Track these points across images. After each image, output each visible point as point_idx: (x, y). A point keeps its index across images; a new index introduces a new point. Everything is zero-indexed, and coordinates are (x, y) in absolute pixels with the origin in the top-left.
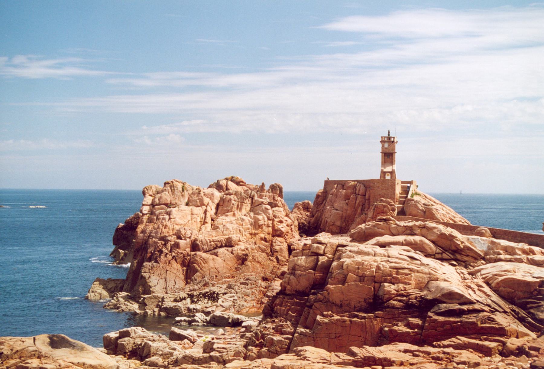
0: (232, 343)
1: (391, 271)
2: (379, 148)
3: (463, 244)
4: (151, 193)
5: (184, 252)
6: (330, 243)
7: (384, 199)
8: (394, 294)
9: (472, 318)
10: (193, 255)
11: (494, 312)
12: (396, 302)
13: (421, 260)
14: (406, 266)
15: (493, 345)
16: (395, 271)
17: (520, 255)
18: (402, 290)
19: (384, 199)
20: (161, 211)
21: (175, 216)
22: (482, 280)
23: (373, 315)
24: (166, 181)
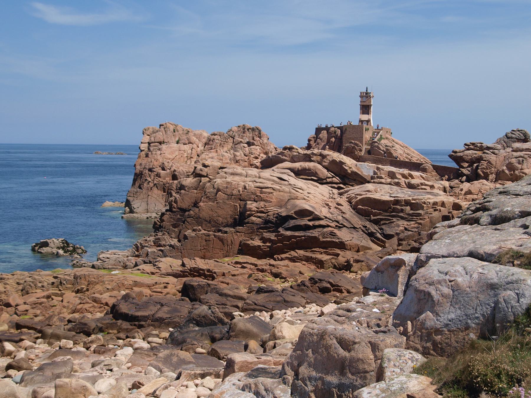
0: (116, 253)
1: (255, 190)
2: (358, 102)
3: (351, 169)
4: (149, 133)
5: (164, 181)
6: (212, 165)
7: (353, 141)
8: (254, 211)
9: (315, 233)
10: (171, 183)
11: (342, 227)
12: (256, 218)
13: (289, 181)
14: (270, 186)
15: (325, 257)
16: (260, 189)
17: (399, 179)
18: (262, 208)
19: (353, 141)
20: (155, 147)
21: (165, 152)
22: (346, 199)
23: (234, 230)
24: (161, 123)
